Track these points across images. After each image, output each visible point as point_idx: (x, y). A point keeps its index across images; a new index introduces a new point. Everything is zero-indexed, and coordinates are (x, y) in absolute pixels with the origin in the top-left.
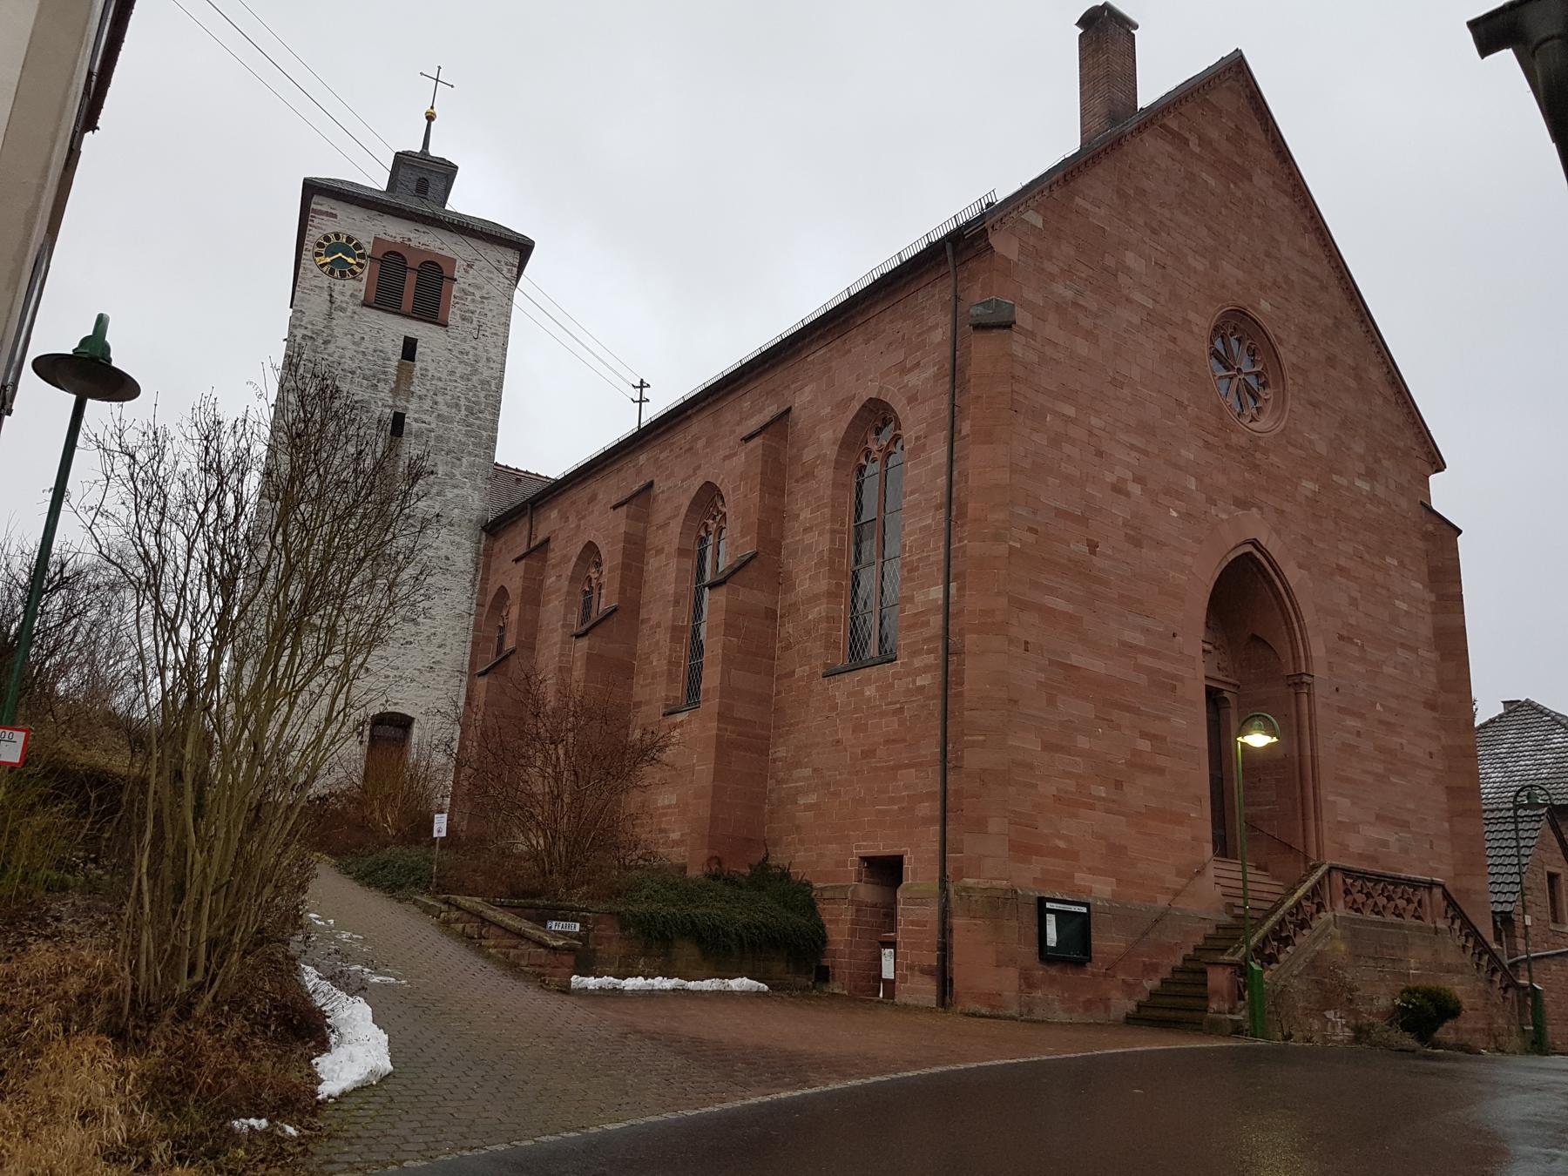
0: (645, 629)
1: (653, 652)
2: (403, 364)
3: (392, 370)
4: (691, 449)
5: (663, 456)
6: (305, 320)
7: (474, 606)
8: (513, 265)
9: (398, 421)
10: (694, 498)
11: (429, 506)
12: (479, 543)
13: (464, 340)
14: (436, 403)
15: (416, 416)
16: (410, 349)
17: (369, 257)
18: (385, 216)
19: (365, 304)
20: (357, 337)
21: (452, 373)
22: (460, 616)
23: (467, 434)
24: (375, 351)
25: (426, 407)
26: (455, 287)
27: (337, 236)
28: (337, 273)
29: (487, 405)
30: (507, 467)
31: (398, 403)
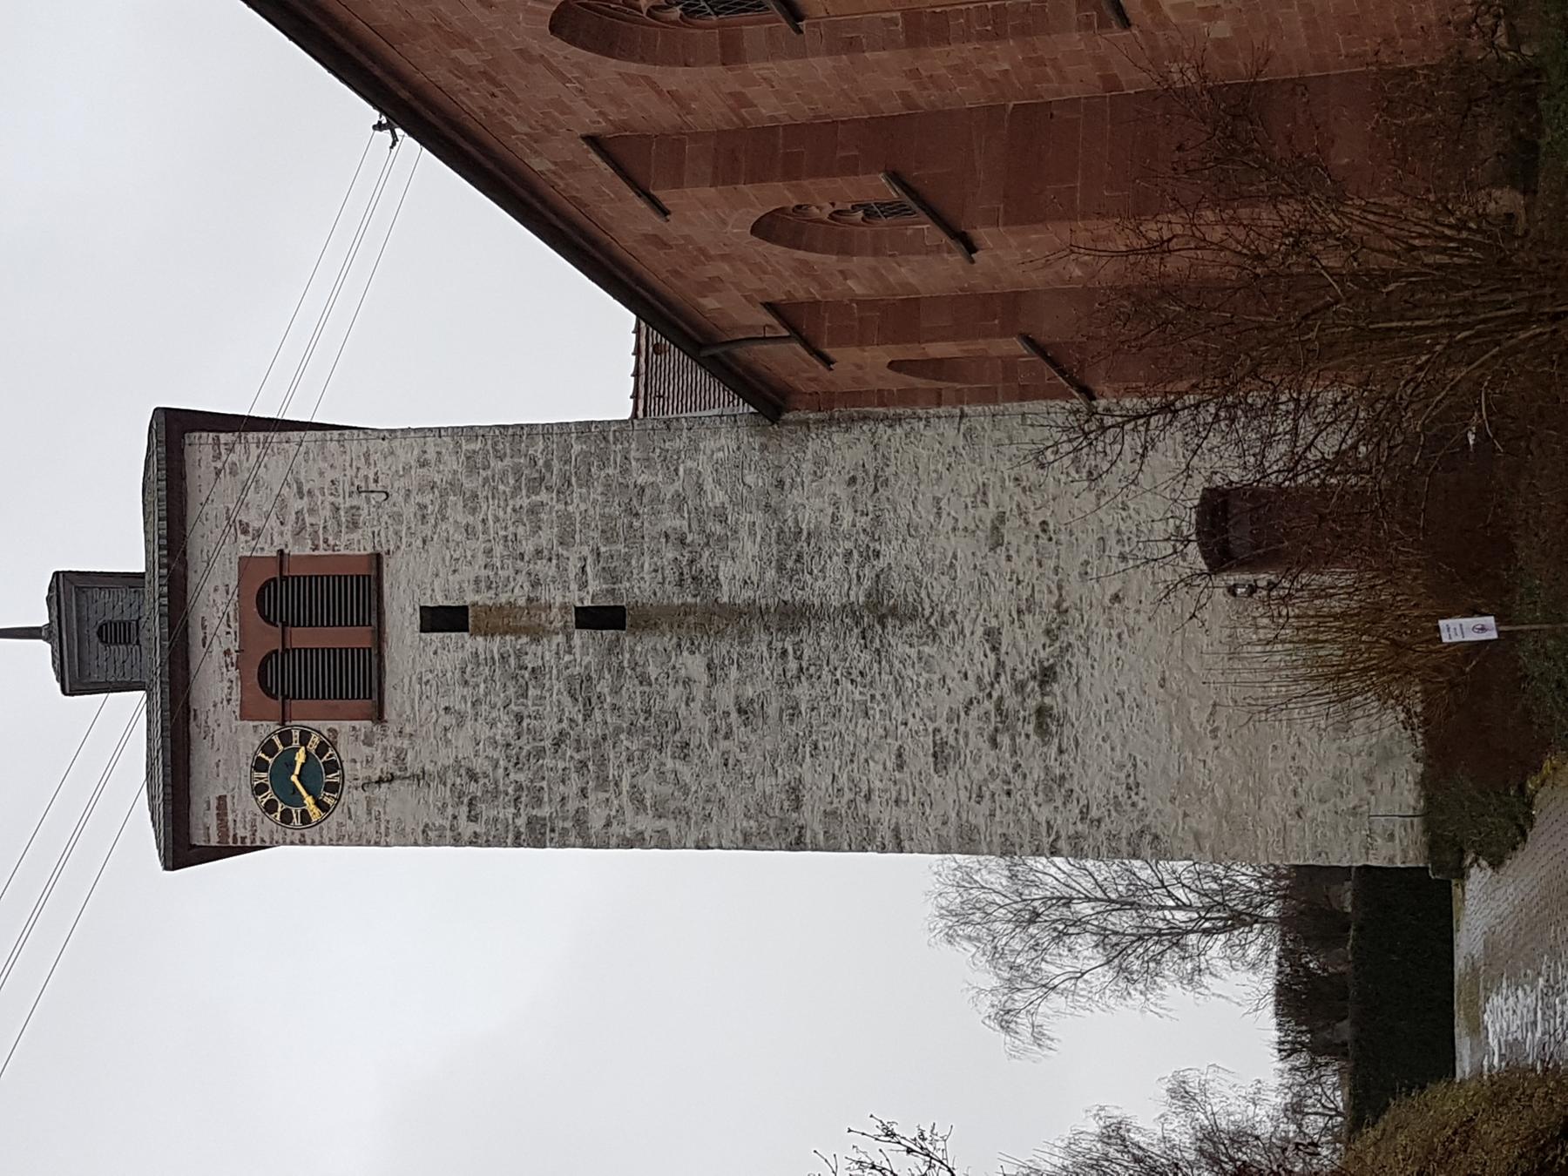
1: (979, 74)
2: (476, 626)
3: (495, 644)
5: (521, 128)
7: (942, 411)
8: (217, 442)
9: (592, 618)
10: (599, 52)
11: (752, 534)
12: (806, 423)
13: (397, 517)
14: (538, 552)
15: (574, 586)
16: (443, 619)
17: (283, 724)
18: (194, 706)
19: (378, 716)
20: (447, 720)
21: (469, 530)
22: (969, 434)
23: (587, 483)
24: (466, 683)
25: (552, 571)
26: (294, 550)
27: (259, 790)
28: (333, 778)
29: (517, 453)
30: (636, 374)
31: (558, 624)
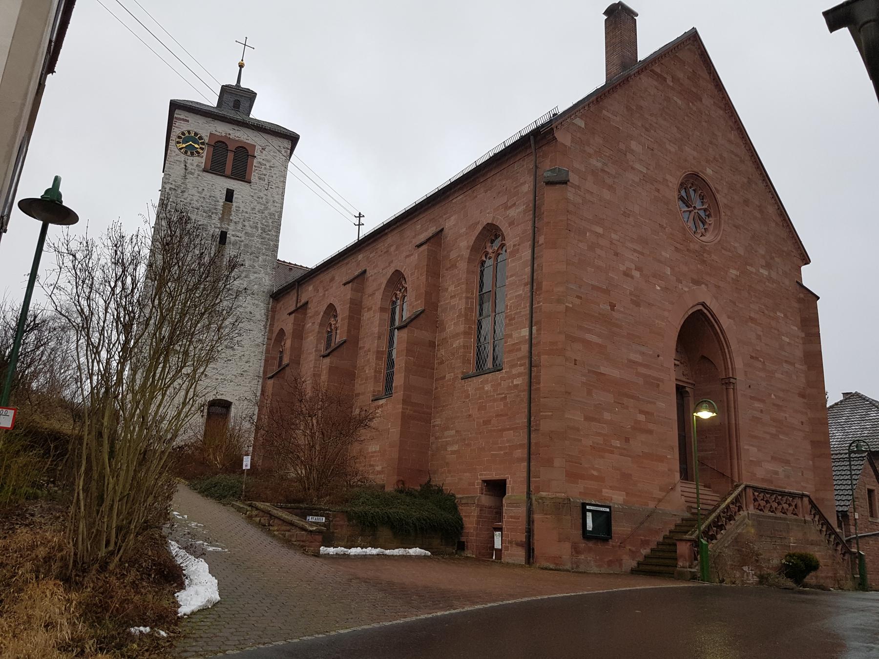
0: (362, 353)
1: (366, 365)
2: (226, 204)
3: (220, 208)
4: (387, 251)
5: (371, 255)
6: (171, 179)
7: (266, 339)
9: (223, 236)
10: (389, 279)
11: (240, 284)
12: (269, 304)
13: (260, 191)
14: (244, 226)
15: (233, 233)
16: (230, 195)
17: (207, 144)
18: (216, 121)
19: (205, 170)
20: (200, 189)
21: (253, 209)
22: (258, 345)
23: (262, 243)
24: (210, 197)
25: (239, 228)
26: (255, 161)
27: (189, 132)
28: (189, 153)
29: (273, 227)
30: (284, 262)
31: (223, 226)
